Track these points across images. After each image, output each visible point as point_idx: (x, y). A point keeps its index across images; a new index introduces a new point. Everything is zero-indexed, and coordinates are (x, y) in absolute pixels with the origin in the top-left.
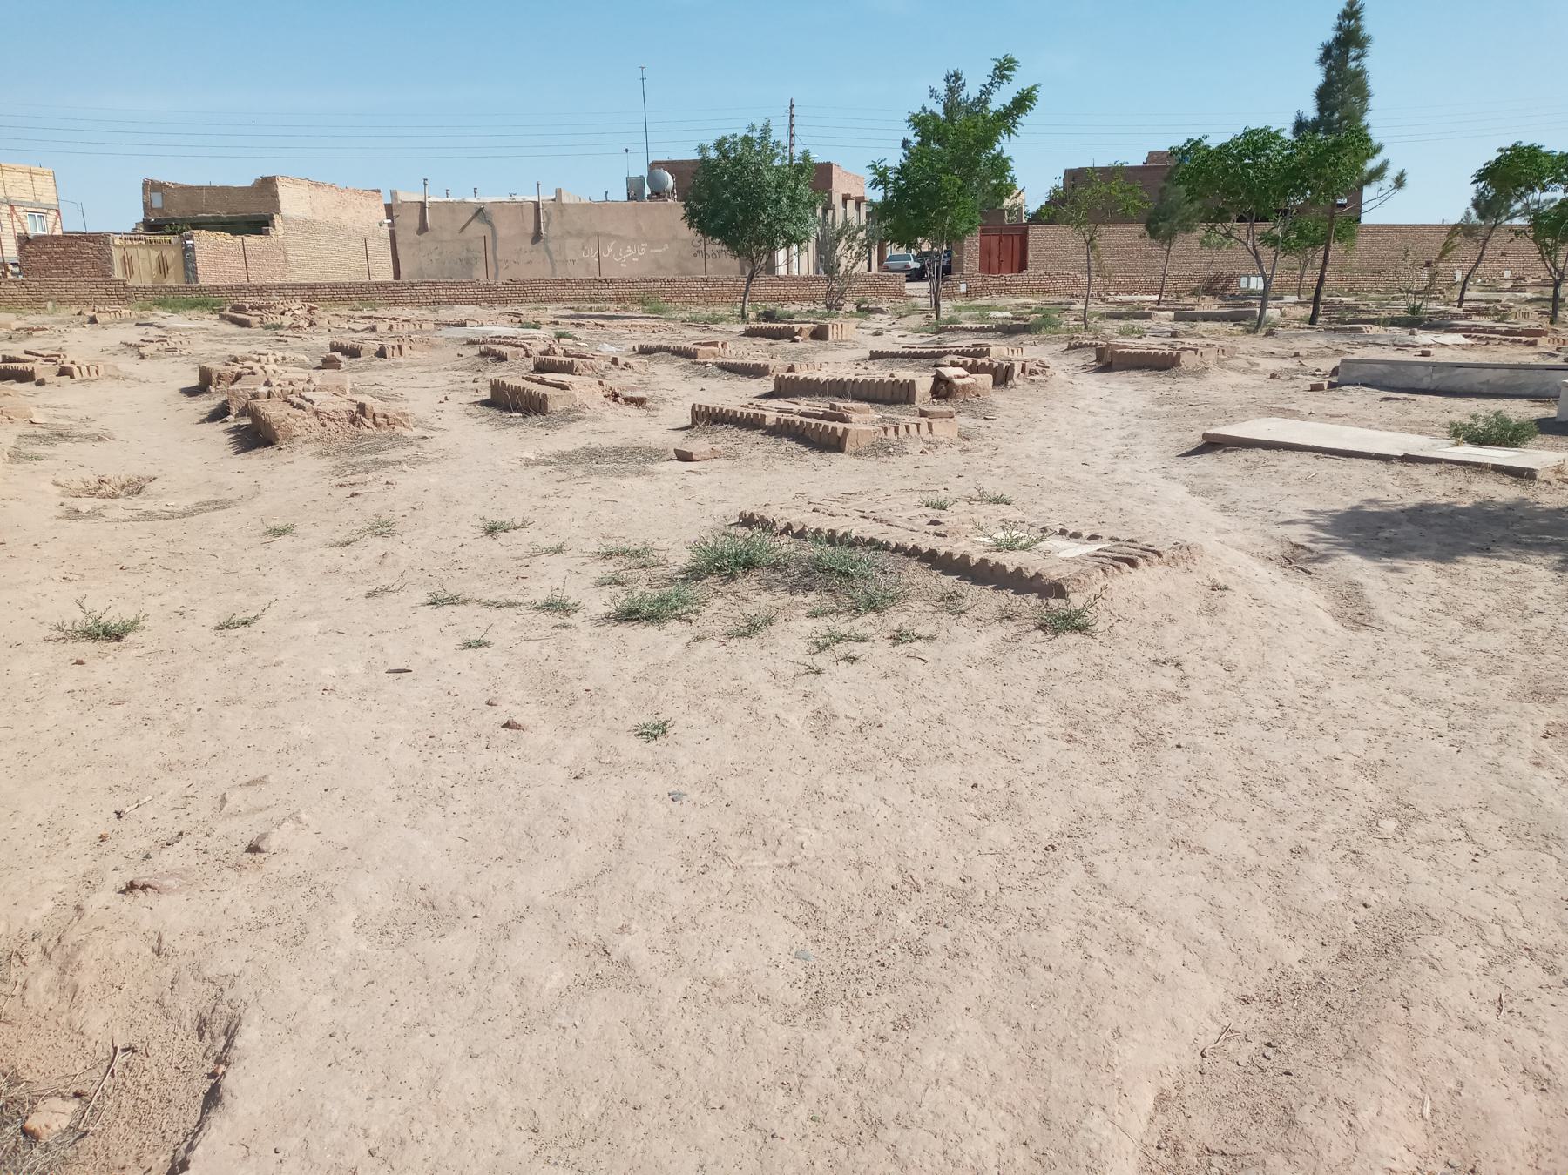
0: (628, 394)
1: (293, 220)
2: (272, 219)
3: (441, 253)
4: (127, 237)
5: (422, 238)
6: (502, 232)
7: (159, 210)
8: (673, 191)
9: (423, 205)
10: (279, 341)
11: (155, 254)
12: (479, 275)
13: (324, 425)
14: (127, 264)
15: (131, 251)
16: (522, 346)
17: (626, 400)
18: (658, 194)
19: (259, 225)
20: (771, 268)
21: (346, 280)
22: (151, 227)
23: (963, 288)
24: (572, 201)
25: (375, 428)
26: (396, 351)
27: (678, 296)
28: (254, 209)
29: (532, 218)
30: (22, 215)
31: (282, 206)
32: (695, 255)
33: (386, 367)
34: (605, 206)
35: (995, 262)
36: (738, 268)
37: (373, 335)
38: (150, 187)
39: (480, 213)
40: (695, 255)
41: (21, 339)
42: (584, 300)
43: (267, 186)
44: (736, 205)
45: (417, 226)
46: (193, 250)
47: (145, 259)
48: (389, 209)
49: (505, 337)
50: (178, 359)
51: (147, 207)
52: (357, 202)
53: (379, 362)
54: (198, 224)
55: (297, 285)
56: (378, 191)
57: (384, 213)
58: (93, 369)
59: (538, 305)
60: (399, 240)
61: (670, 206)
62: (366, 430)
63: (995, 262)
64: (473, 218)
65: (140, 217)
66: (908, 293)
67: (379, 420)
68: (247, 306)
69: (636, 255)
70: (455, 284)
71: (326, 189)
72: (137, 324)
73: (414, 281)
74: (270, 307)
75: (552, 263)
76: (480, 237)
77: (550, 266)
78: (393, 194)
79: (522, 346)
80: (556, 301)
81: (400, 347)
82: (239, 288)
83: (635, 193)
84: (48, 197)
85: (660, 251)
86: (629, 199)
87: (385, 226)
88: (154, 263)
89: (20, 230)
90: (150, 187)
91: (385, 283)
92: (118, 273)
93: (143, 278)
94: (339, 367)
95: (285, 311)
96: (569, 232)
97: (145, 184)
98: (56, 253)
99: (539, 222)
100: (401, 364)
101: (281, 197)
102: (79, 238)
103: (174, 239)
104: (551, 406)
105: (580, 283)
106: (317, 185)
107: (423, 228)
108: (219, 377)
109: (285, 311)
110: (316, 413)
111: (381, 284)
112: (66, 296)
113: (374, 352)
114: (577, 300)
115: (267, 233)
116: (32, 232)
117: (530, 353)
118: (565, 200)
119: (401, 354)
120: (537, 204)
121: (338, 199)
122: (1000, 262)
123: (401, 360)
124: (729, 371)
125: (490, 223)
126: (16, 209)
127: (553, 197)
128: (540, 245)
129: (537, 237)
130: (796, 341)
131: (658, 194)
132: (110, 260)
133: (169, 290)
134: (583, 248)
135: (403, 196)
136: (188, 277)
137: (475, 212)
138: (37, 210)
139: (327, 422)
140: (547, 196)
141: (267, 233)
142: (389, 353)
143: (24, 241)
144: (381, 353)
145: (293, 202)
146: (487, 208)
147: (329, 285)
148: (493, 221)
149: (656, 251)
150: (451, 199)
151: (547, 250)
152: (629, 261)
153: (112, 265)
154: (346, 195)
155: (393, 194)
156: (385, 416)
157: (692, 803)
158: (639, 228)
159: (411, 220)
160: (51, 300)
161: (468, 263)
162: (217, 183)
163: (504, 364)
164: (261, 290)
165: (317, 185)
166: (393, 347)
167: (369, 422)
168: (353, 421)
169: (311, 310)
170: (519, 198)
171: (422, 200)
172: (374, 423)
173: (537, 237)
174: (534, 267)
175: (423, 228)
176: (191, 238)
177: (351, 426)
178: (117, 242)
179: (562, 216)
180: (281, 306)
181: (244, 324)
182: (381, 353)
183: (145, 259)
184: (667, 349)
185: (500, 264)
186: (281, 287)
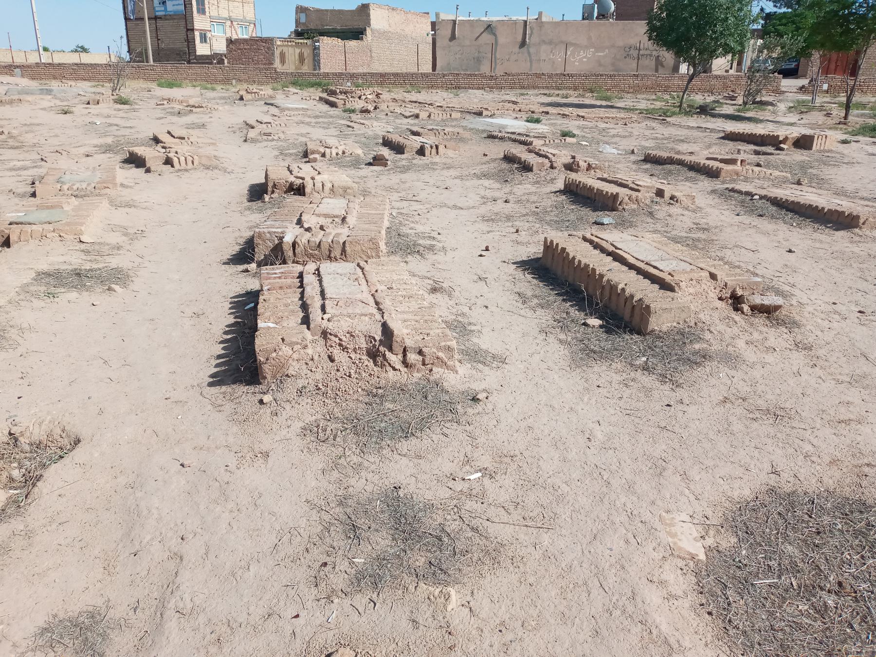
0: (758, 300)
1: (378, 32)
2: (365, 30)
3: (462, 54)
4: (284, 40)
5: (452, 44)
6: (502, 40)
7: (304, 24)
8: (613, 14)
9: (454, 22)
10: (349, 126)
11: (298, 51)
12: (485, 69)
13: (332, 360)
14: (283, 56)
15: (285, 49)
16: (546, 157)
17: (753, 308)
18: (603, 16)
19: (357, 34)
20: (707, 70)
21: (404, 71)
22: (299, 34)
23: (825, 87)
24: (548, 20)
25: (404, 369)
26: (434, 150)
27: (616, 86)
28: (356, 25)
29: (521, 31)
30: (236, 26)
31: (372, 22)
32: (625, 57)
33: (426, 167)
34: (563, 24)
35: (833, 66)
36: (654, 67)
37: (416, 121)
38: (300, 10)
39: (489, 28)
40: (625, 57)
41: (185, 114)
42: (552, 88)
43: (364, 9)
44: (692, 23)
45: (450, 36)
46: (319, 49)
47: (292, 54)
48: (433, 25)
49: (519, 134)
50: (270, 144)
51: (297, 22)
52: (415, 20)
53: (419, 160)
54: (324, 33)
55: (374, 73)
56: (428, 13)
57: (430, 27)
58: (189, 159)
59: (523, 91)
60: (437, 45)
61: (612, 24)
62: (391, 373)
63: (833, 66)
64: (484, 31)
65: (292, 27)
66: (783, 89)
67: (412, 357)
68: (338, 91)
69: (584, 57)
70: (471, 75)
71: (398, 12)
72: (265, 103)
73: (445, 73)
74: (352, 93)
75: (531, 62)
76: (488, 44)
77: (529, 64)
78: (437, 15)
79: (546, 157)
80: (534, 88)
81: (437, 147)
82: (340, 75)
83: (587, 15)
84: (250, 16)
85: (602, 54)
86: (583, 19)
87: (430, 35)
88: (297, 57)
89: (229, 35)
90: (300, 10)
91: (427, 74)
92: (277, 64)
93: (290, 67)
94: (385, 165)
95: (361, 95)
96: (544, 41)
97: (297, 8)
98: (245, 49)
99: (526, 34)
100: (436, 163)
101: (372, 17)
102: (257, 40)
103: (309, 42)
104: (655, 324)
105: (550, 76)
106: (393, 9)
107: (453, 37)
108: (275, 186)
109: (361, 95)
110: (325, 334)
111: (425, 74)
112: (243, 76)
113: (415, 150)
114: (548, 88)
115: (362, 39)
116: (234, 37)
117: (555, 165)
118: (544, 19)
119: (437, 153)
120: (525, 22)
121: (404, 18)
122: (837, 66)
123: (437, 159)
124: (791, 211)
125: (495, 35)
126: (234, 23)
127: (536, 17)
128: (524, 49)
129: (523, 44)
130: (782, 149)
131: (603, 16)
132: (273, 54)
133: (301, 75)
134: (551, 52)
135: (443, 17)
136: (315, 65)
137: (486, 27)
138: (245, 23)
139: (337, 352)
140: (533, 16)
141: (362, 39)
142: (427, 152)
143: (230, 42)
144: (421, 152)
145: (378, 19)
146: (494, 25)
147: (393, 74)
148: (497, 33)
149: (600, 54)
150: (472, 18)
151: (529, 53)
152: (581, 61)
153: (274, 57)
154: (409, 16)
155: (437, 15)
156: (420, 352)
157: (589, 444)
158: (590, 38)
159: (446, 32)
160: (235, 79)
161: (478, 61)
162: (336, 8)
163: (530, 174)
164: (353, 76)
165: (393, 9)
166: (431, 147)
167: (394, 359)
168: (373, 354)
169: (378, 95)
170: (514, 18)
171: (454, 19)
172: (405, 363)
173: (523, 44)
174: (518, 64)
175: (453, 37)
176: (318, 41)
177: (371, 364)
178: (279, 43)
179: (541, 30)
180: (359, 92)
181: (333, 105)
182: (421, 152)
183: (292, 54)
184: (681, 163)
185: (498, 61)
186: (365, 74)
